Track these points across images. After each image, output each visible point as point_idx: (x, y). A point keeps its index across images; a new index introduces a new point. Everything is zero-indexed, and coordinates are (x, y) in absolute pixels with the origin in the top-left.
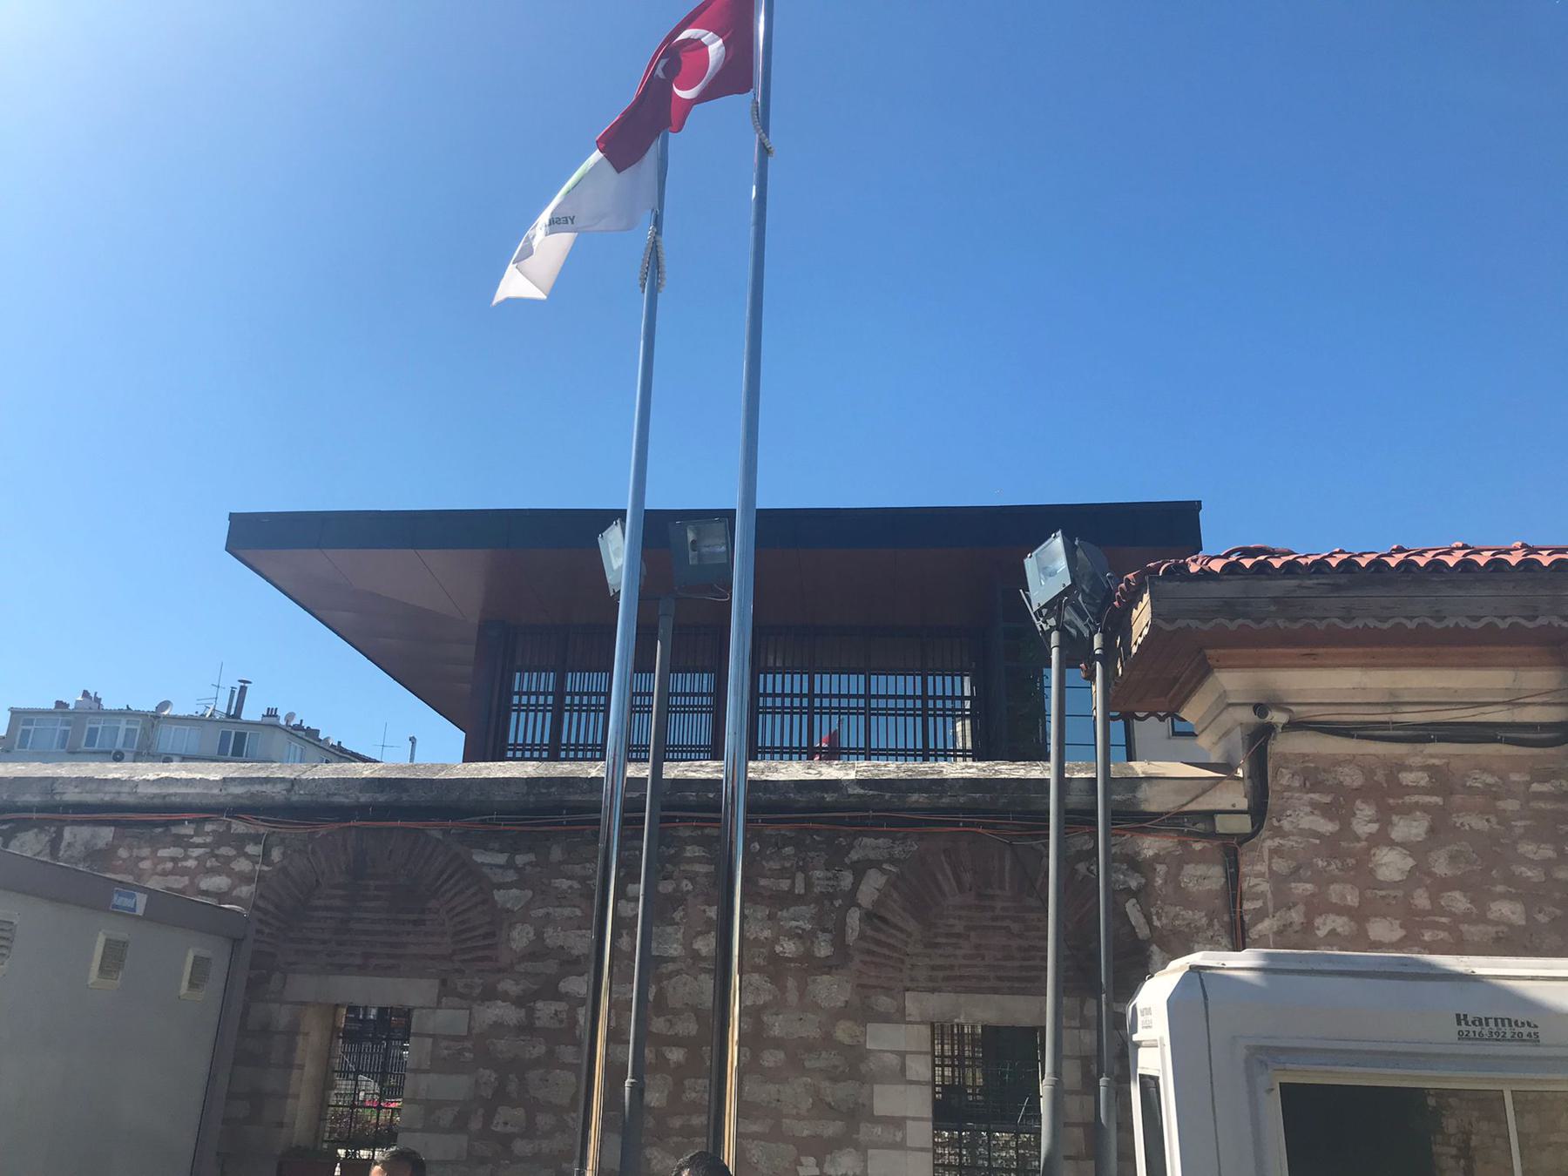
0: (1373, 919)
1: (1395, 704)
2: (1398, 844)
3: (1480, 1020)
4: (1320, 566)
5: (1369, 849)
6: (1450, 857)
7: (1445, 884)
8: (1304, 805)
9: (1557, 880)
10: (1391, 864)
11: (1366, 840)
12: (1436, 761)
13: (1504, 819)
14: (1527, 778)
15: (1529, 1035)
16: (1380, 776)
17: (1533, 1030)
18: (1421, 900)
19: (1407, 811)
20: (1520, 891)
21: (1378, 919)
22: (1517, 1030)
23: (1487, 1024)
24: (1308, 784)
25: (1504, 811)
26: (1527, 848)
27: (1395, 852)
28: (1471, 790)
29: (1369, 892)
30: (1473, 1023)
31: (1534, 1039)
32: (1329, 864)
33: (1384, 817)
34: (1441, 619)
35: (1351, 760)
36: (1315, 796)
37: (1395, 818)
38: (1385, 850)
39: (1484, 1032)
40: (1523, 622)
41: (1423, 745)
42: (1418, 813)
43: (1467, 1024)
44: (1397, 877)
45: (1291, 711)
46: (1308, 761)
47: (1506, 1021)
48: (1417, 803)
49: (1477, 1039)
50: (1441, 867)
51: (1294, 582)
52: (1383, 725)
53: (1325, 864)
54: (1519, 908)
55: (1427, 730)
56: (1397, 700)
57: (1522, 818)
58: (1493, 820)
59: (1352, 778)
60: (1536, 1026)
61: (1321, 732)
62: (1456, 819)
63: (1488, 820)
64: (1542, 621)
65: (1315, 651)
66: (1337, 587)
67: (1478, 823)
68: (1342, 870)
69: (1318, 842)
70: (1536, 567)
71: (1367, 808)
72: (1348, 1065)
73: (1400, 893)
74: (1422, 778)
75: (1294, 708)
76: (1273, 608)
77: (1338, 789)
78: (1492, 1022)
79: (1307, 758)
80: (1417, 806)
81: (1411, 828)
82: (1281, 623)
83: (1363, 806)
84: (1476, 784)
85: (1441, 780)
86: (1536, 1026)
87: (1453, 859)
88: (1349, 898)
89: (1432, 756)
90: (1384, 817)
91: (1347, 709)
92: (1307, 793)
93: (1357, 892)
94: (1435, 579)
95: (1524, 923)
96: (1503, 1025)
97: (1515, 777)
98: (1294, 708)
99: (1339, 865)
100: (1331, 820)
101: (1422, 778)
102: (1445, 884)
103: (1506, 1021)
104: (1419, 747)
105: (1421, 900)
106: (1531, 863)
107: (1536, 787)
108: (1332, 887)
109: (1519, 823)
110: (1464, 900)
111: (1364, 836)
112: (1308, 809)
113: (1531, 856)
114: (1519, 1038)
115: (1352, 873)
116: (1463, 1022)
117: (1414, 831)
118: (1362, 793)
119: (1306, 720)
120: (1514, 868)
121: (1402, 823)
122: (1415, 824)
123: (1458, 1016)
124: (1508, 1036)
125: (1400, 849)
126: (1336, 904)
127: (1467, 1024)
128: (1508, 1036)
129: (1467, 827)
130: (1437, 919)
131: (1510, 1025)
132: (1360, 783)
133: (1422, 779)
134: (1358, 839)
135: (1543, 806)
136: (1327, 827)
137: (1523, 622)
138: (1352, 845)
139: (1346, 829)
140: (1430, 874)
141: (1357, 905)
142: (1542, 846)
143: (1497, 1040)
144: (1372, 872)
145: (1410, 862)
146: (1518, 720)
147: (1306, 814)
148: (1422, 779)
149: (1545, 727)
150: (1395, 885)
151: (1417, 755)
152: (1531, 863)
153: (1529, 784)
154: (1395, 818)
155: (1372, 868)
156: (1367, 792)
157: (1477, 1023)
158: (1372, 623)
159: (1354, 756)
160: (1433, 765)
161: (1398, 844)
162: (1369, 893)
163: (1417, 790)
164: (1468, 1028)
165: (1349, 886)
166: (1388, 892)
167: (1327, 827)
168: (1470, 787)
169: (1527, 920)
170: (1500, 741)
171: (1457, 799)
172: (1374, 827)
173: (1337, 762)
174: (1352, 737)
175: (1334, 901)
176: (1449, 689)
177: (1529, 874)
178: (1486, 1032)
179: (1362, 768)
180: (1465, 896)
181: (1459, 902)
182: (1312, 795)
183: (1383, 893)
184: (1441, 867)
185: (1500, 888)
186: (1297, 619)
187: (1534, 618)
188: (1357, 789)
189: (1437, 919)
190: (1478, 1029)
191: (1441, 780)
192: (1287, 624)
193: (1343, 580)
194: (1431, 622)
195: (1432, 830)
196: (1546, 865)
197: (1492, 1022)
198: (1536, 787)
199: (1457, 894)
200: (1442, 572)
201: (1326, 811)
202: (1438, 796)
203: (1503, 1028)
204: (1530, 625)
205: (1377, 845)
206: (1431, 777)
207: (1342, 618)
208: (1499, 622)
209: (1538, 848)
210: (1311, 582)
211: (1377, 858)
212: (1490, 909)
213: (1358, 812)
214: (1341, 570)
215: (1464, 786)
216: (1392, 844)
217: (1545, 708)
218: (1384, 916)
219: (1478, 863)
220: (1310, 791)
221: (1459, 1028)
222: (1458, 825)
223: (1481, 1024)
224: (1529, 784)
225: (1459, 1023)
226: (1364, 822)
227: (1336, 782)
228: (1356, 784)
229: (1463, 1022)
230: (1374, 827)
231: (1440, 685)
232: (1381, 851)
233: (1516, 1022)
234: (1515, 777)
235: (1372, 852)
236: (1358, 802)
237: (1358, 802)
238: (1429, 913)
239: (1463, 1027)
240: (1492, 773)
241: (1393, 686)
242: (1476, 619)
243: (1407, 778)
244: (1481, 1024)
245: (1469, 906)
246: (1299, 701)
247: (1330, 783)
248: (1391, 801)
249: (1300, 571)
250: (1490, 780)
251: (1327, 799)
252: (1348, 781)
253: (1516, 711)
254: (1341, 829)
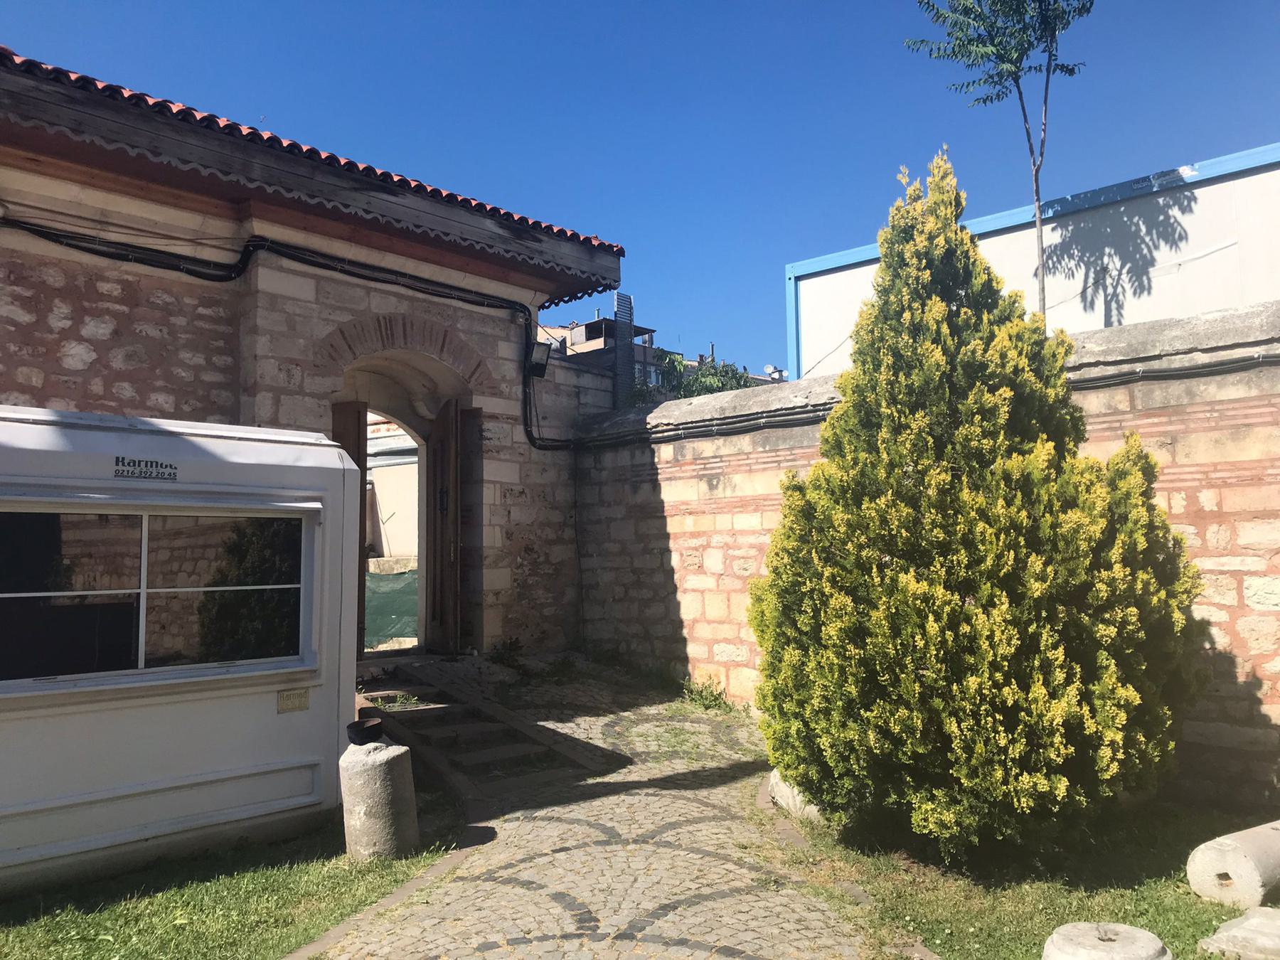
0: (54, 399)
1: (104, 223)
2: (87, 341)
3: (134, 462)
4: (59, 75)
5: (60, 340)
6: (127, 355)
7: (120, 376)
8: (5, 295)
9: (202, 382)
10: (76, 356)
11: (58, 333)
12: (130, 278)
13: (173, 332)
14: (196, 302)
15: (170, 474)
16: (81, 281)
17: (172, 471)
18: (97, 387)
19: (97, 314)
20: (174, 387)
21: (57, 399)
22: (161, 470)
23: (139, 466)
24: (12, 277)
25: (174, 325)
26: (185, 355)
27: (82, 346)
28: (153, 306)
29: (53, 376)
30: (129, 464)
31: (173, 478)
32: (21, 349)
33: (78, 317)
34: (157, 154)
35: (57, 264)
36: (17, 289)
37: (87, 319)
38: (74, 344)
39: (135, 471)
40: (219, 174)
41: (121, 262)
42: (107, 317)
43: (123, 465)
44: (80, 366)
45: (7, 208)
46: (14, 257)
47: (154, 464)
48: (108, 309)
49: (129, 477)
50: (118, 361)
51: (31, 83)
52: (92, 239)
53: (17, 349)
54: (171, 399)
55: (126, 250)
56: (105, 220)
57: (186, 333)
58: (165, 330)
59: (55, 279)
60: (176, 468)
61: (31, 232)
62: (136, 326)
63: (161, 330)
64: (233, 178)
65: (42, 158)
66: (73, 100)
67: (152, 331)
68: (33, 356)
69: (13, 329)
70: (237, 133)
71: (64, 306)
72: (16, 495)
73: (79, 380)
74: (116, 289)
75: (10, 206)
76: (6, 101)
77: (42, 286)
78: (143, 464)
79: (15, 255)
80: (108, 311)
81: (98, 329)
82: (13, 118)
83: (61, 304)
84: (158, 301)
85: (131, 295)
86: (176, 468)
87: (129, 357)
88: (34, 379)
89: (127, 273)
90: (78, 317)
91: (60, 218)
92: (11, 285)
93: (42, 375)
94: (157, 118)
95: (173, 411)
96: (151, 466)
97: (187, 300)
98: (10, 206)
99: (30, 352)
100: (29, 312)
101: (116, 289)
102: (120, 376)
103: (154, 464)
104: (119, 263)
105: (97, 387)
106: (187, 367)
107: (201, 310)
108: (20, 369)
109: (183, 336)
110: (131, 389)
111: (57, 330)
112: (10, 299)
113: (188, 361)
114: (160, 477)
115: (41, 359)
116: (120, 464)
117: (101, 331)
118: (63, 293)
119: (21, 219)
120: (173, 369)
121: (92, 323)
122: (103, 325)
123: (118, 458)
124: (154, 475)
125: (87, 344)
126: (21, 383)
127: (123, 465)
128: (154, 475)
129: (144, 333)
130: (106, 402)
131: (157, 466)
132: (62, 285)
133: (116, 290)
134: (51, 331)
135: (203, 325)
136: (25, 318)
137: (219, 174)
138: (45, 336)
139: (41, 322)
140: (107, 367)
141: (40, 386)
142: (197, 355)
143: (145, 478)
144: (58, 360)
145: (94, 356)
146: (198, 256)
147: (7, 304)
148: (116, 290)
149: (217, 265)
150: (76, 373)
151: (115, 270)
152: (187, 367)
153: (196, 307)
154: (87, 319)
155: (60, 358)
156: (66, 293)
157: (132, 464)
158: (99, 141)
159: (60, 261)
160: (127, 280)
161: (87, 341)
162: (53, 377)
163: (108, 298)
164: (124, 468)
165: (36, 370)
166: (71, 378)
167: (25, 318)
168: (153, 302)
169: (175, 409)
170: (181, 270)
171: (141, 311)
172: (68, 323)
173: (43, 262)
174: (61, 243)
175: (20, 381)
176: (149, 220)
177: (184, 374)
178: (137, 471)
179: (65, 272)
180: (132, 387)
181: (126, 390)
182: (15, 288)
183: (66, 378)
184: (118, 361)
185: (159, 383)
186: (27, 118)
187: (228, 174)
188: (59, 290)
189: (106, 402)
190: (131, 469)
191: (131, 295)
192: (19, 120)
193: (79, 94)
194: (150, 156)
195: (116, 333)
196: (197, 369)
197: (143, 464)
198: (201, 310)
199: (126, 385)
200: (166, 116)
201: (25, 303)
202: (127, 306)
203: (151, 470)
204: (225, 178)
205: (67, 339)
206: (123, 290)
207: (73, 130)
208: (201, 169)
209: (194, 356)
210: (48, 87)
211: (65, 349)
212: (149, 398)
213: (55, 309)
214: (79, 84)
215: (148, 301)
216: (81, 340)
217: (219, 250)
218: (63, 397)
219: (148, 362)
220: (13, 283)
221: (117, 468)
222: (137, 331)
223: (134, 465)
224: (196, 307)
225: (117, 464)
226: (59, 317)
227: (40, 280)
228: (57, 285)
229: (120, 464)
230: (68, 323)
231: (145, 215)
232: (70, 344)
233: (162, 464)
234: (187, 300)
235: (62, 344)
236: (57, 301)
237: (57, 301)
238: (101, 398)
239: (120, 467)
240: (169, 292)
241: (105, 208)
242: (186, 162)
243: (104, 287)
244: (134, 465)
245: (134, 394)
246: (15, 200)
247: (33, 279)
248: (86, 304)
249: (39, 73)
250: (169, 299)
251: (28, 293)
252: (50, 281)
253: (199, 248)
254: (37, 321)
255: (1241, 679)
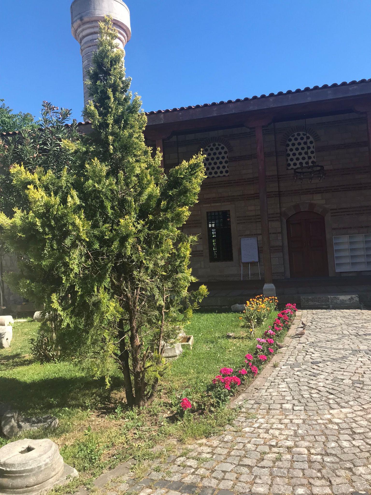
210: (28, 468)
255: (191, 269)
